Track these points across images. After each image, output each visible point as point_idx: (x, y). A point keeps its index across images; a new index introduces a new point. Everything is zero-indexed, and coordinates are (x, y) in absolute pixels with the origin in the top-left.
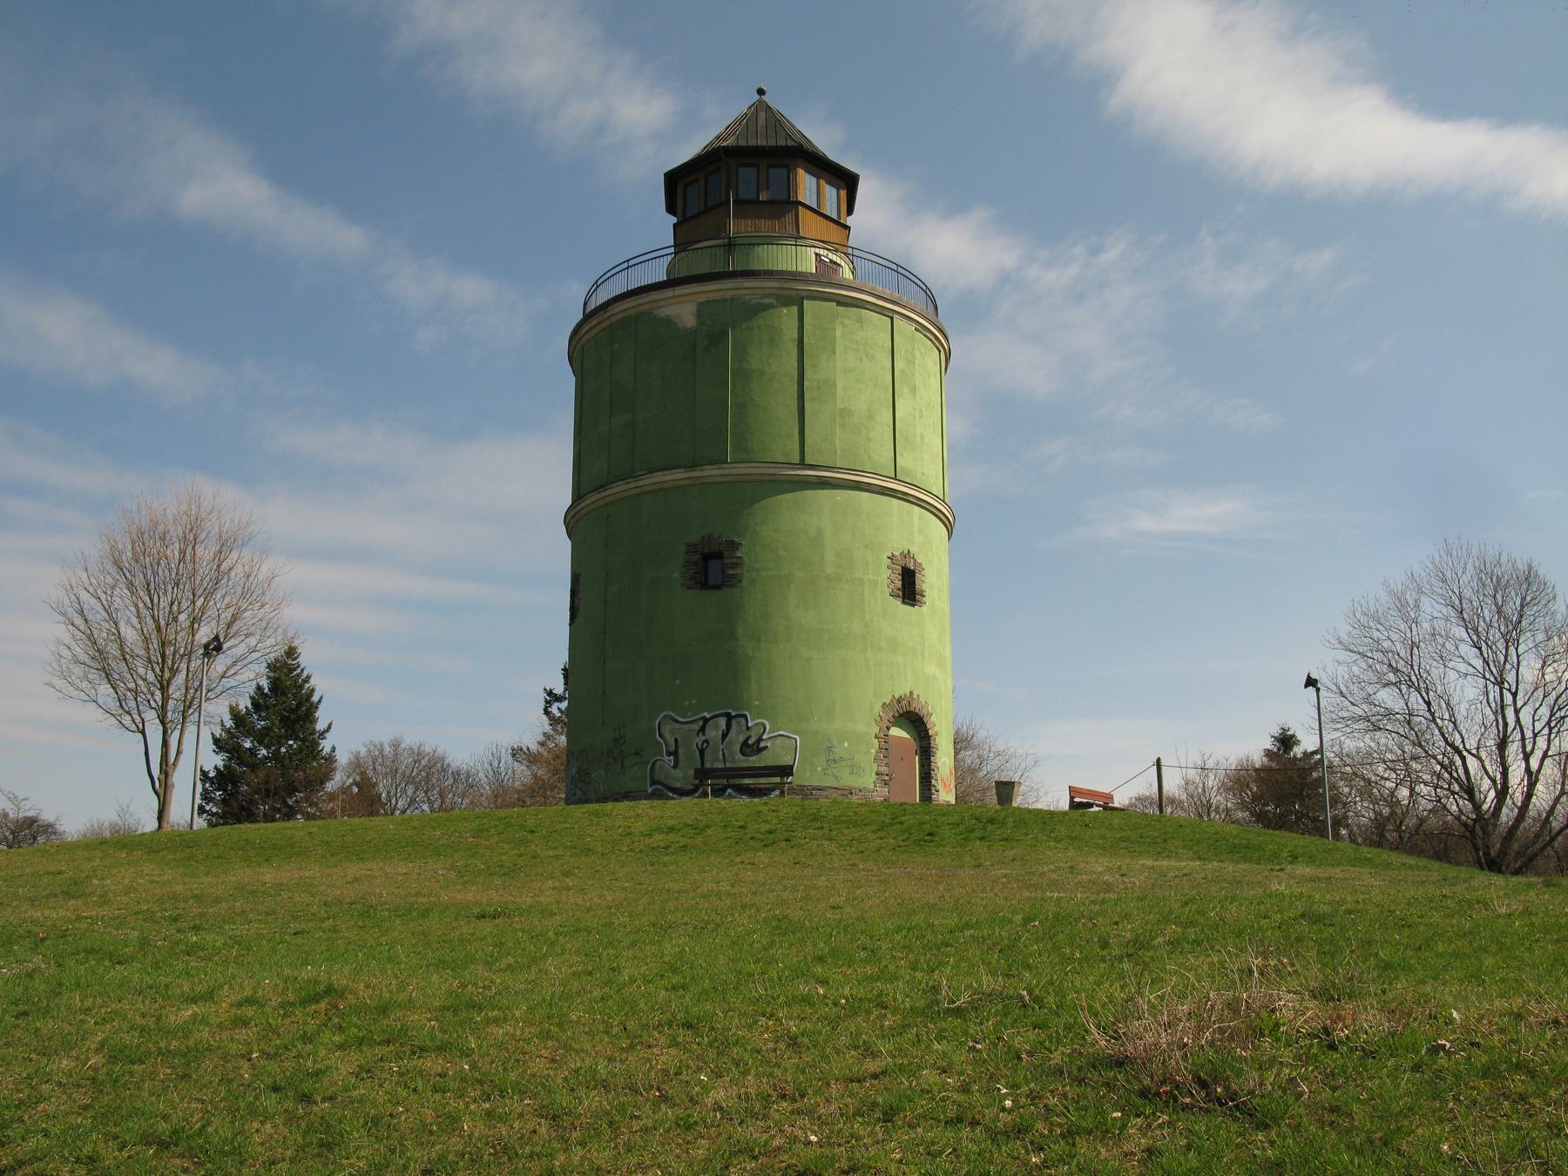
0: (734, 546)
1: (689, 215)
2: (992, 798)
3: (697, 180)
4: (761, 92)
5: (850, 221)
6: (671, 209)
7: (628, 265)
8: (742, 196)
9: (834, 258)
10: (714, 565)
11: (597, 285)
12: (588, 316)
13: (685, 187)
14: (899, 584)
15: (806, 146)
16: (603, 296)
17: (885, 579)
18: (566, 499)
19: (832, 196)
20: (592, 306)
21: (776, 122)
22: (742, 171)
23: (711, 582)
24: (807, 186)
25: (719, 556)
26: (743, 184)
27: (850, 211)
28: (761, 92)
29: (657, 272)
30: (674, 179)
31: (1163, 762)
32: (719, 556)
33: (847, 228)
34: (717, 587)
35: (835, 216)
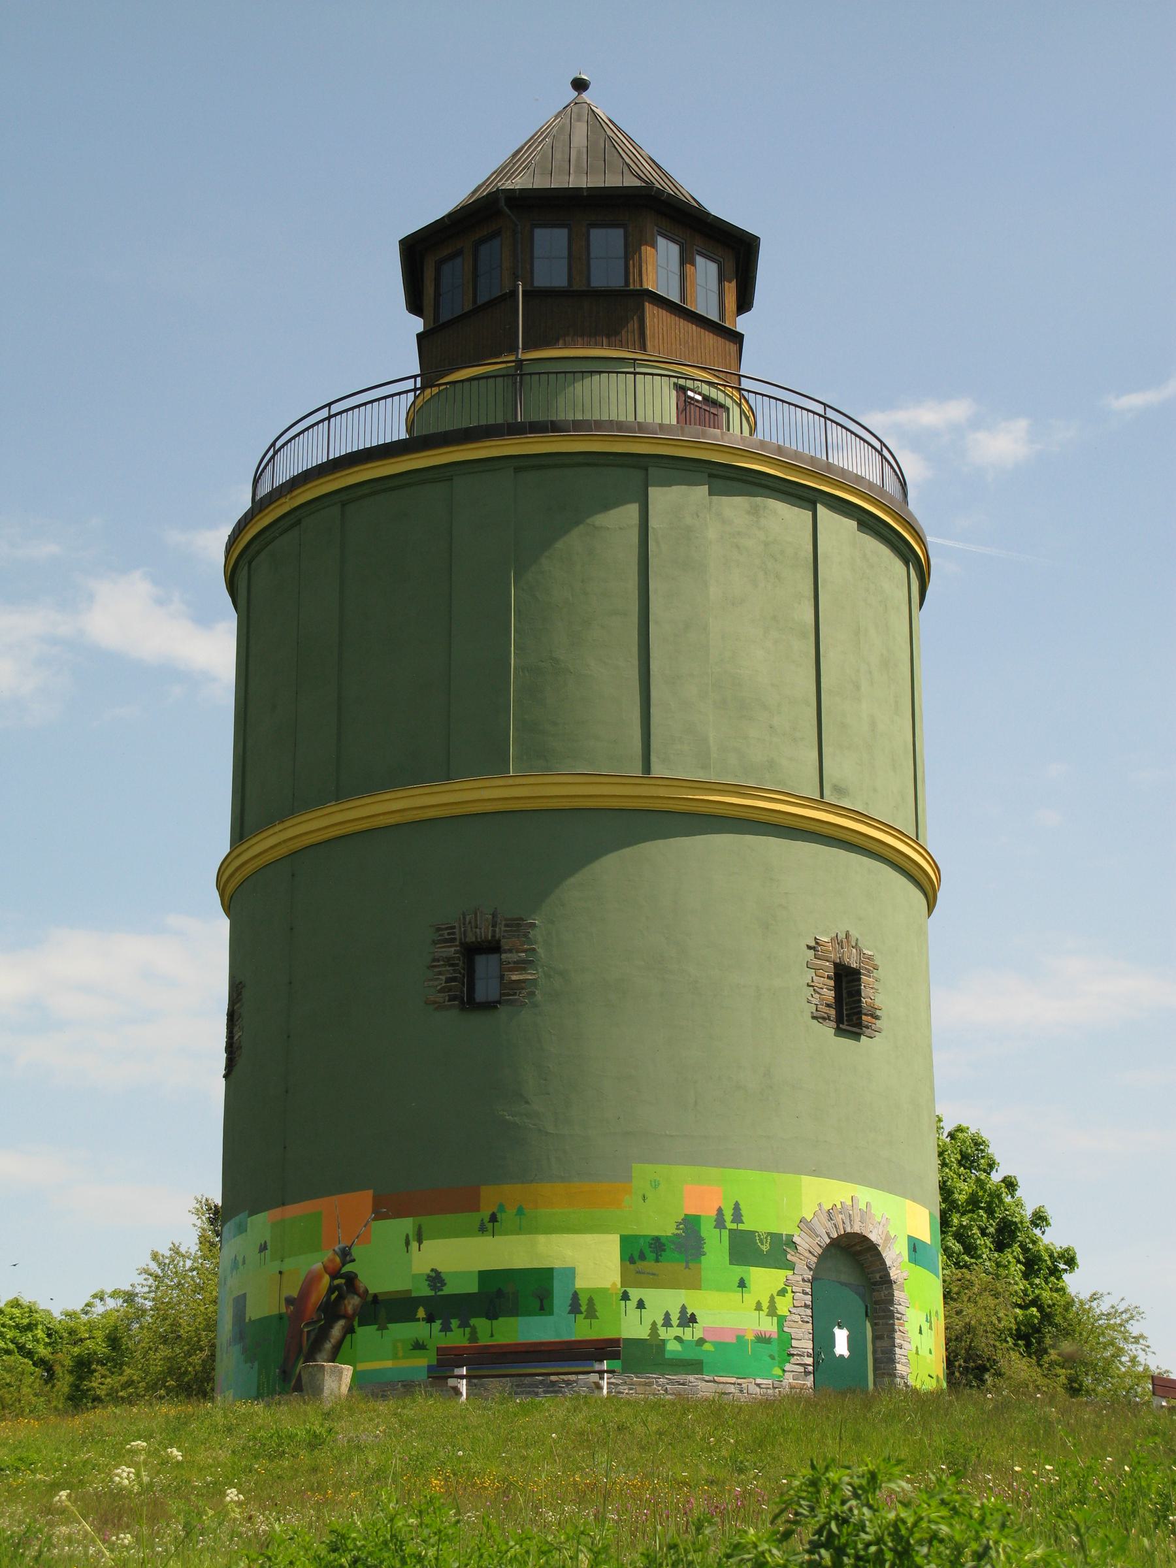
0: (518, 926)
1: (445, 316)
2: (1028, 1213)
3: (459, 253)
4: (580, 85)
5: (742, 323)
6: (415, 305)
7: (329, 413)
8: (542, 280)
9: (713, 393)
10: (485, 965)
11: (274, 449)
12: (259, 506)
13: (438, 271)
14: (830, 995)
15: (659, 183)
16: (288, 467)
17: (805, 989)
18: (222, 845)
19: (706, 284)
20: (265, 489)
21: (606, 139)
22: (539, 233)
23: (480, 996)
24: (661, 265)
25: (493, 947)
26: (553, 268)
27: (744, 303)
28: (580, 85)
29: (389, 424)
30: (420, 253)
31: (424, 1229)
32: (493, 947)
33: (737, 338)
34: (490, 1006)
35: (714, 316)
